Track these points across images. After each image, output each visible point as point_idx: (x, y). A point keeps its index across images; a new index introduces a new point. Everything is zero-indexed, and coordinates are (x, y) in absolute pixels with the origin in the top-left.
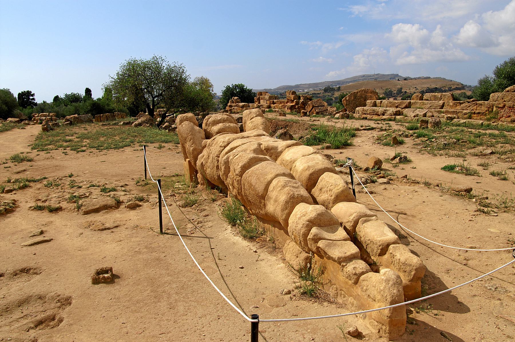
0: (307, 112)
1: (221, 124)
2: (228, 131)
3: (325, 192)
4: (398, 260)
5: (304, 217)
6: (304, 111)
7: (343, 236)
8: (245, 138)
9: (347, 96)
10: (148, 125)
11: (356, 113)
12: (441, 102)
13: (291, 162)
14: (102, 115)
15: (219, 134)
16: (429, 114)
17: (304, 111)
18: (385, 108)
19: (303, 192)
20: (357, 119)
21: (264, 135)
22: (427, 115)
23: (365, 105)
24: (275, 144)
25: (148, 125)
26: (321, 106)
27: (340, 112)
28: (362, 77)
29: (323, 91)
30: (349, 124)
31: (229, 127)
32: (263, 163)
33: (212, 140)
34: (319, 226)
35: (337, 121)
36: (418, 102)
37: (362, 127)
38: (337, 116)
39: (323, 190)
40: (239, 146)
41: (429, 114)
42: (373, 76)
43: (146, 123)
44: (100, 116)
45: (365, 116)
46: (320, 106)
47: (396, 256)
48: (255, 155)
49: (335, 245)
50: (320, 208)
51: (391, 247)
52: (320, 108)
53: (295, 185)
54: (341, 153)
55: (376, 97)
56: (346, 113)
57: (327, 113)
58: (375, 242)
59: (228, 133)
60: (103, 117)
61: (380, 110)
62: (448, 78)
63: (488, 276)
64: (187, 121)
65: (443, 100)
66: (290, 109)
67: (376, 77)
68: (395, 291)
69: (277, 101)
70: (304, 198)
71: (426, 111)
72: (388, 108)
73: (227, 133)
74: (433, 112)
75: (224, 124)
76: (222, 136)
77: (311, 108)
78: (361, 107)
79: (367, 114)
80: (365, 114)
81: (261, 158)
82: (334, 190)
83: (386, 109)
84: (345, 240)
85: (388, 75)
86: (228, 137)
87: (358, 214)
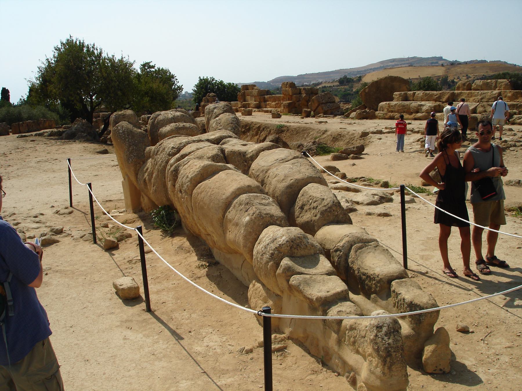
0: (310, 112)
1: (173, 125)
2: (182, 134)
3: (308, 211)
4: (402, 300)
5: (272, 245)
6: (306, 109)
7: (327, 270)
8: (203, 141)
9: (367, 87)
10: (85, 134)
11: (378, 110)
12: (496, 92)
13: (263, 171)
14: (21, 123)
15: (167, 138)
16: (480, 109)
17: (306, 109)
18: (419, 103)
19: (275, 210)
20: (380, 118)
21: (230, 137)
22: (478, 111)
23: (392, 99)
24: (243, 149)
25: (85, 134)
26: (330, 102)
27: (357, 109)
28: (391, 62)
29: (338, 84)
30: (370, 125)
31: (184, 128)
32: (222, 174)
33: (158, 146)
34: (292, 257)
35: (353, 121)
36: (464, 93)
37: (386, 128)
38: (353, 114)
39: (306, 208)
40: (193, 152)
41: (480, 109)
42: (407, 60)
43: (82, 132)
44: (19, 124)
45: (391, 114)
46: (328, 103)
47: (400, 294)
48: (210, 163)
49: (314, 281)
50: (295, 231)
51: (393, 283)
52: (329, 105)
53: (264, 201)
54: (354, 165)
55: (407, 87)
56: (365, 112)
57: (338, 111)
58: (372, 277)
59: (180, 136)
60: (22, 125)
61: (414, 104)
62: (489, 58)
63: (485, 300)
64: (124, 121)
65: (499, 90)
66: (287, 108)
67: (410, 61)
68: (390, 341)
69: (270, 97)
70: (276, 218)
71: (476, 105)
72: (423, 103)
73: (178, 136)
74: (486, 106)
75: (176, 124)
76: (172, 139)
77: (317, 105)
78: (385, 102)
79: (395, 112)
80: (392, 112)
81: (219, 166)
82: (319, 207)
83: (421, 103)
84: (329, 274)
85: (428, 59)
86: (184, 139)
87: (350, 239)
